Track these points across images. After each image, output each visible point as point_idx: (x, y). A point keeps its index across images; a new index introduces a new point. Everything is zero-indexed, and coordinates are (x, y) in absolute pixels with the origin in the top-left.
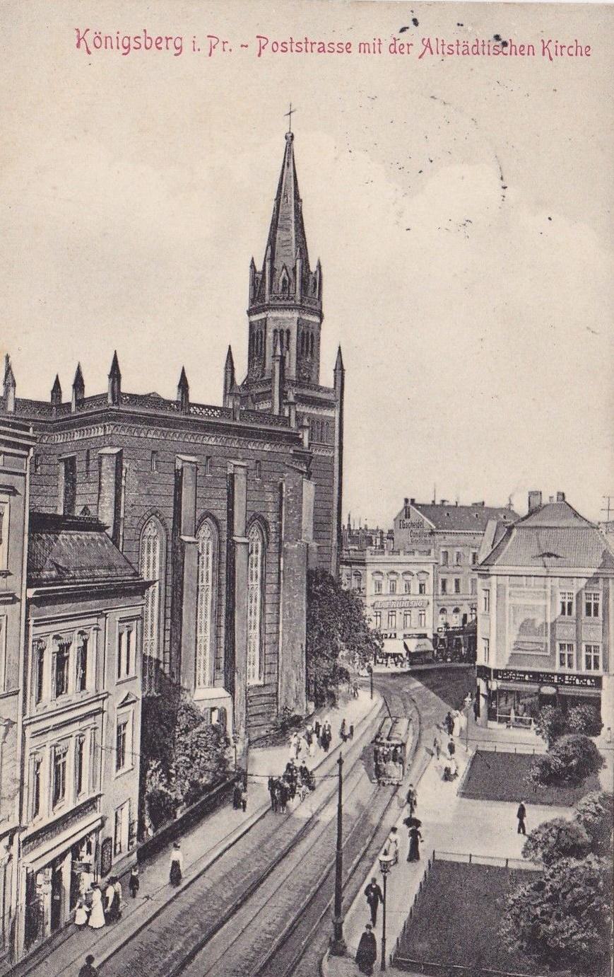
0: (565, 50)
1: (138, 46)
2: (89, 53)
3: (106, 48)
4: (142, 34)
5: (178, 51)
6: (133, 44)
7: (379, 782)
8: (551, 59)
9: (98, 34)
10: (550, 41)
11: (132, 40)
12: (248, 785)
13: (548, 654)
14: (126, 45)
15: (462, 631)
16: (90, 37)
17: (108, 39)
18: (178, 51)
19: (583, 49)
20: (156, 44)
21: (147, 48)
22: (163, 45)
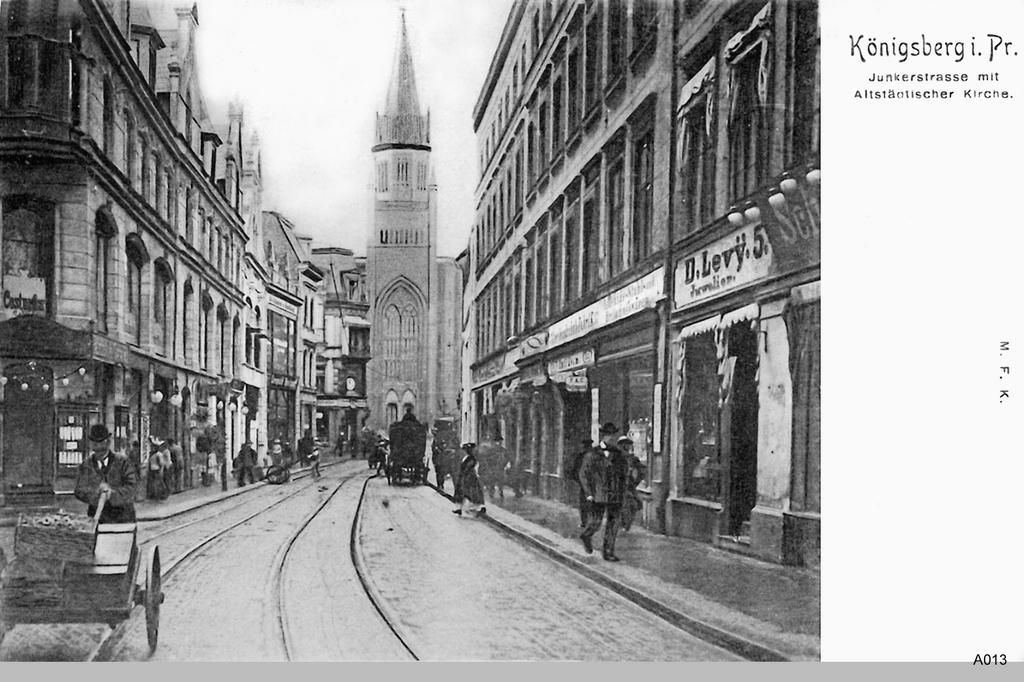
0: (951, 49)
1: (916, 52)
2: (863, 60)
3: (881, 54)
4: (920, 41)
5: (959, 57)
6: (911, 50)
7: (426, 414)
8: (863, 60)
9: (872, 41)
10: (861, 37)
11: (909, 46)
12: (65, 285)
13: (253, 335)
14: (903, 51)
15: (614, 428)
16: (864, 44)
17: (884, 46)
18: (959, 57)
19: (933, 48)
20: (936, 50)
21: (925, 54)
22: (943, 51)
